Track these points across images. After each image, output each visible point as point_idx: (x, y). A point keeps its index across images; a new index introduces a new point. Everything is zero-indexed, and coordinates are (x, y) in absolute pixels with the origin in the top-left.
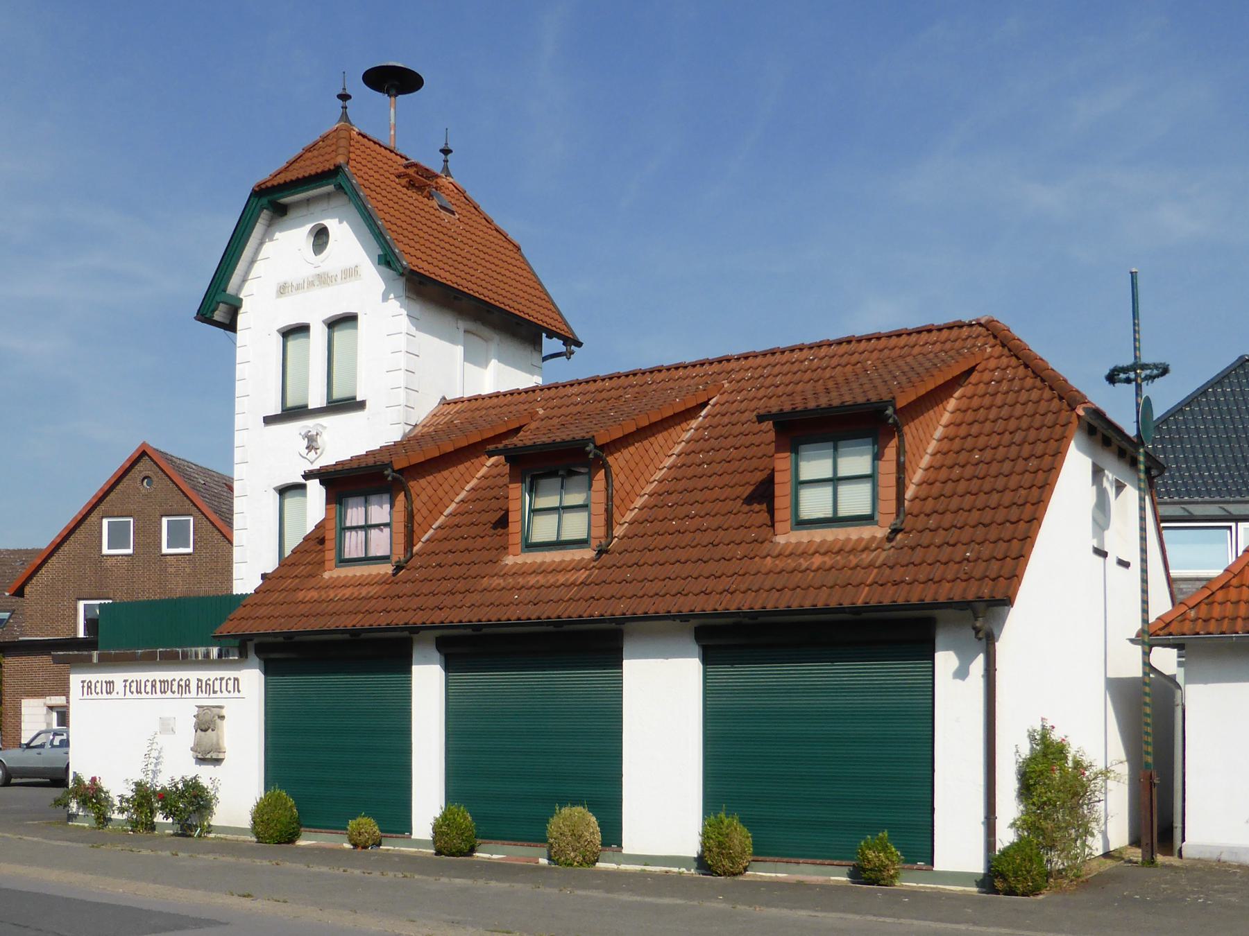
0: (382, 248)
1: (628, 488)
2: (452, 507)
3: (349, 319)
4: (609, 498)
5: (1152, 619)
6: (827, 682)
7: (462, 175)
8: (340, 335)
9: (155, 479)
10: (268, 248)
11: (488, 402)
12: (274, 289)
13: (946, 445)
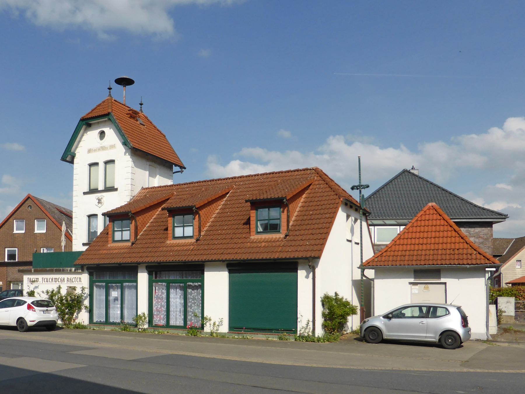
0: (124, 140)
1: (205, 220)
2: (149, 224)
3: (112, 161)
4: (200, 224)
5: (364, 261)
6: (266, 282)
7: (146, 112)
8: (109, 166)
9: (32, 206)
10: (84, 138)
11: (157, 189)
12: (87, 151)
13: (302, 209)
